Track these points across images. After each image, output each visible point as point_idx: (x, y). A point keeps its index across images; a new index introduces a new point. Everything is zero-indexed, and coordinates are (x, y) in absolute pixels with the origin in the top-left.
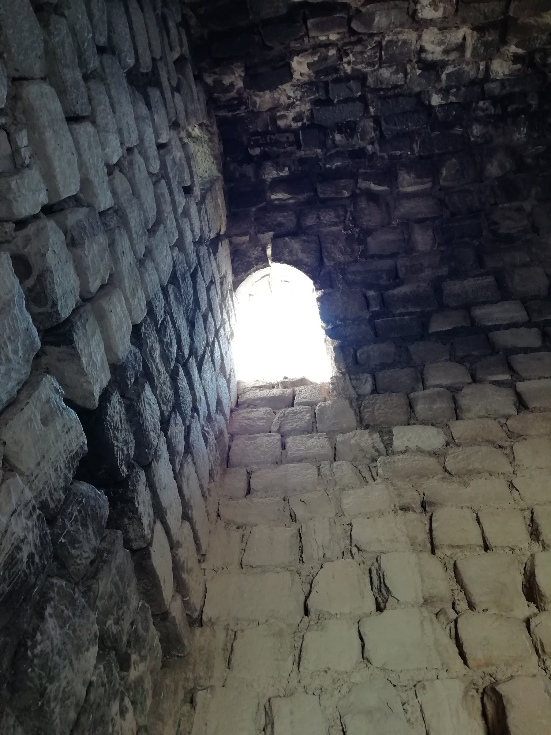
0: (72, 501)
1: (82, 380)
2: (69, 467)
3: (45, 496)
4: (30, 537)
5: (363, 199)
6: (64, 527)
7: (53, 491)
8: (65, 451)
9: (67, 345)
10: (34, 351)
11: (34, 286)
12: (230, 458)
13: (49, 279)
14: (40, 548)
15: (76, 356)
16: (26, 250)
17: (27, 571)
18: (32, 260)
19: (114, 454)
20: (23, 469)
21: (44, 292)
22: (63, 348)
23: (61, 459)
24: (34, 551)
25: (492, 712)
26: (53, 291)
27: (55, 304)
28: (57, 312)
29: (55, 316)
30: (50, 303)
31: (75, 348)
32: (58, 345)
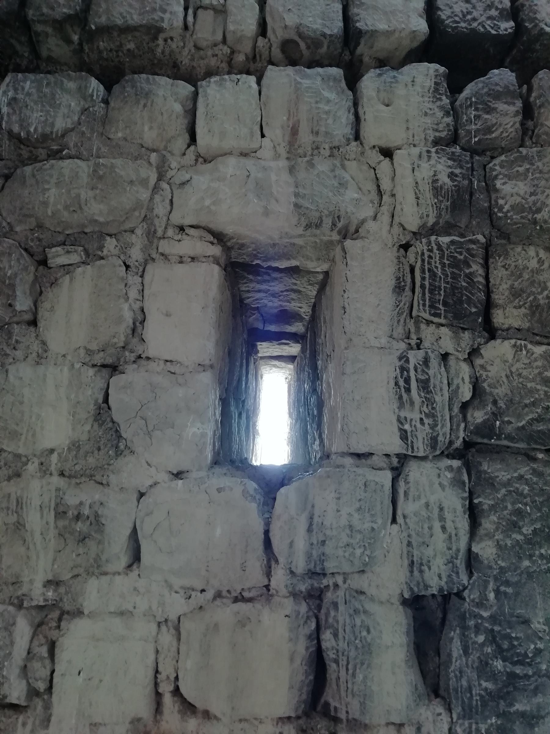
0: (462, 112)
1: (397, 35)
2: (437, 99)
3: (432, 135)
4: (440, 167)
5: (42, 690)
6: (469, 132)
7: (435, 127)
8: (423, 96)
9: (361, 37)
10: (340, 81)
11: (307, 44)
12: (30, 639)
13: (305, 29)
14: (456, 164)
15: (374, 33)
16: (279, 38)
17: (456, 183)
18: (287, 36)
19: (482, 34)
20: (398, 143)
21: (312, 39)
22: (363, 41)
23: (425, 104)
24: (450, 170)
25: (400, 484)
26: (315, 31)
27: (324, 35)
28: (331, 36)
29: (333, 38)
30: (322, 38)
31: (367, 32)
32: (358, 44)
